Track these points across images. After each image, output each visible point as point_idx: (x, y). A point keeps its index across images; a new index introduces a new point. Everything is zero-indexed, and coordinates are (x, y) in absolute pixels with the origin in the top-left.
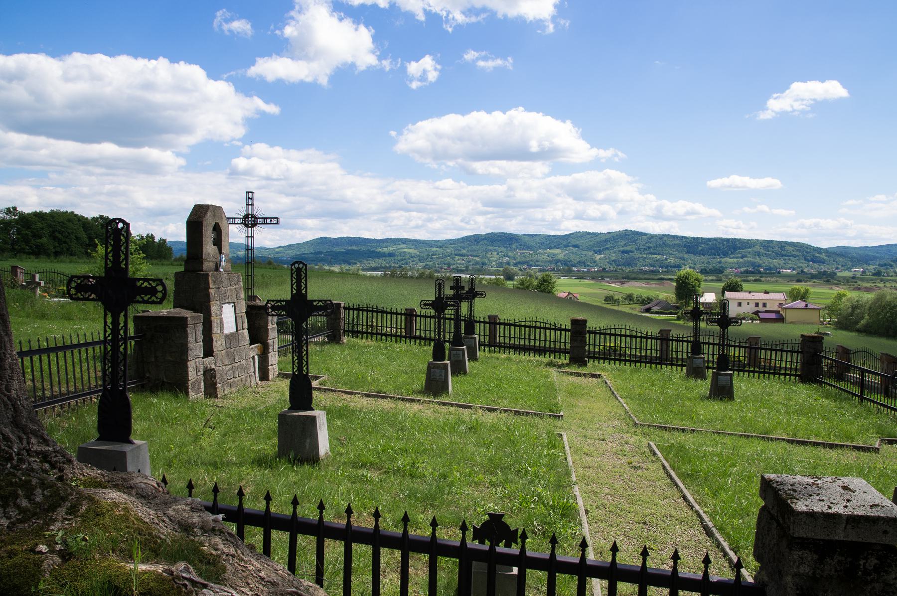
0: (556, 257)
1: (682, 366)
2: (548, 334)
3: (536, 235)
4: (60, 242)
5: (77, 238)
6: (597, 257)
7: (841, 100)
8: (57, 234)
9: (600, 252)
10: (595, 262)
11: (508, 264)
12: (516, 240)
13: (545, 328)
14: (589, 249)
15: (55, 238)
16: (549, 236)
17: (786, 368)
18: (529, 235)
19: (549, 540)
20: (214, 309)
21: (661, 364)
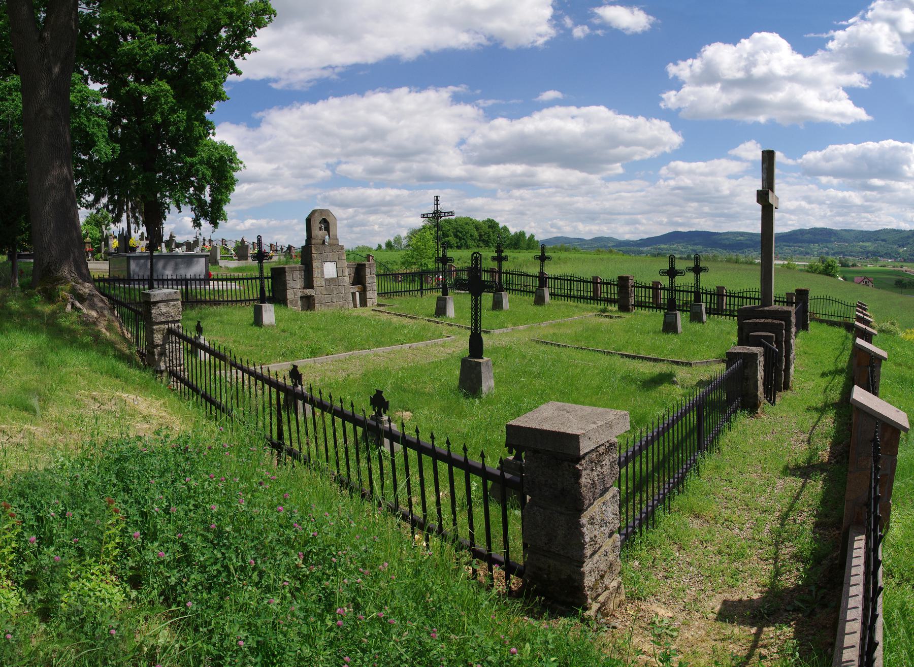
0: (868, 249)
1: (686, 311)
2: (681, 295)
3: (851, 230)
4: (460, 239)
5: (471, 236)
6: (901, 250)
7: (868, 122)
8: (458, 234)
9: (903, 246)
10: (899, 254)
11: (827, 254)
12: (835, 234)
13: (577, 281)
14: (894, 243)
15: (456, 236)
16: (862, 231)
17: (645, 302)
18: (845, 230)
19: (585, 447)
20: (315, 264)
21: (718, 314)
